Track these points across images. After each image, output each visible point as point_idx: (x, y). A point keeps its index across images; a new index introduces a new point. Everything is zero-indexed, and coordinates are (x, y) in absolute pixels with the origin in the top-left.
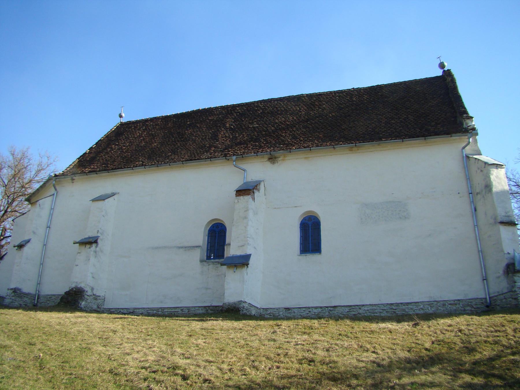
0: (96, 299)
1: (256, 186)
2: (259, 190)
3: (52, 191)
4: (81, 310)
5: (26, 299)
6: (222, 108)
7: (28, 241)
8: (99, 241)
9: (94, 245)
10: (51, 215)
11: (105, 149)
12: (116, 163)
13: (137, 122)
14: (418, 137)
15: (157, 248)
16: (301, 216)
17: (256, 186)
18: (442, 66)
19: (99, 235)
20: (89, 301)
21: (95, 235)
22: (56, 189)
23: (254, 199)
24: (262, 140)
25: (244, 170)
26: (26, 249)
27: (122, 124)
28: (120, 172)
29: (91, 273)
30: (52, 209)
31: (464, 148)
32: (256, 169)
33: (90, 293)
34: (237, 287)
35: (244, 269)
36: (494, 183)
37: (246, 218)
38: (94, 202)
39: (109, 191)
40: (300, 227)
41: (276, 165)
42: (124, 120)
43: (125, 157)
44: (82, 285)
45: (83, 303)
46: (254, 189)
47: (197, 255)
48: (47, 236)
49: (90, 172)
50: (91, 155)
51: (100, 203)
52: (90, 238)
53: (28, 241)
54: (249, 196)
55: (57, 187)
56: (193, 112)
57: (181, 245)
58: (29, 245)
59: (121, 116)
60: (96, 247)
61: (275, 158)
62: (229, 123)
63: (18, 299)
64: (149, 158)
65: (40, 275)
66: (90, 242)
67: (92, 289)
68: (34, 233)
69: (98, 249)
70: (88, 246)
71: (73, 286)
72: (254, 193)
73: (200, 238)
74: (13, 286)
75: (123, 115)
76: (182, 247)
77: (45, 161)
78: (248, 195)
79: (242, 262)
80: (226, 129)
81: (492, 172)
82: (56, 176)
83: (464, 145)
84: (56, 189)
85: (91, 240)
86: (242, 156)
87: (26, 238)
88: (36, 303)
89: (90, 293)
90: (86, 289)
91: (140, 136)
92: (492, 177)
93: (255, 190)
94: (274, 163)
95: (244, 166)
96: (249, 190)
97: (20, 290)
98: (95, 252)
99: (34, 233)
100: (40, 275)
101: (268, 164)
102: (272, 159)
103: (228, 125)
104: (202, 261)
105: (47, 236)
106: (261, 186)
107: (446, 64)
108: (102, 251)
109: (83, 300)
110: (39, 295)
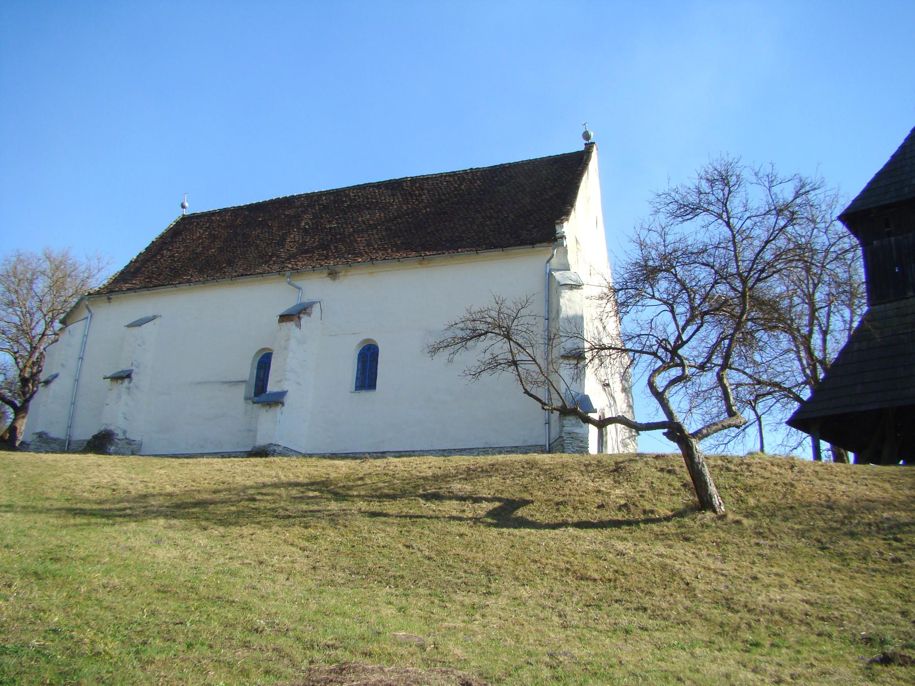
0: (130, 444)
1: (305, 309)
2: (309, 315)
3: (86, 313)
4: (110, 454)
5: (54, 445)
6: (307, 196)
7: (56, 376)
8: (133, 375)
9: (127, 381)
10: (84, 343)
11: (155, 256)
12: (162, 277)
13: (203, 215)
14: (496, 247)
15: (200, 383)
16: (359, 345)
17: (305, 309)
18: (586, 136)
19: (133, 368)
20: (120, 446)
21: (130, 368)
22: (90, 311)
23: (299, 326)
24: (332, 247)
25: (299, 288)
26: (52, 385)
27: (185, 219)
28: (161, 290)
29: (119, 412)
30: (86, 336)
31: (548, 261)
32: (314, 287)
33: (121, 436)
34: (270, 426)
35: (278, 409)
36: (563, 308)
37: (286, 348)
38: (131, 329)
39: (150, 314)
40: (359, 359)
41: (337, 281)
42: (186, 212)
43: (175, 268)
44: (112, 428)
45: (113, 448)
46: (300, 313)
47: (241, 392)
48: (79, 370)
49: (129, 289)
50: (137, 265)
51: (136, 329)
52: (123, 371)
53: (56, 376)
54: (292, 323)
55: (91, 309)
56: (278, 201)
57: (225, 380)
58: (57, 380)
59: (183, 207)
60: (130, 383)
61: (336, 273)
62: (306, 221)
63: (44, 445)
64: (201, 271)
65: (72, 417)
66: (123, 376)
67: (125, 432)
68: (63, 366)
69: (131, 385)
70: (120, 382)
71: (103, 428)
72: (299, 318)
73: (246, 370)
74: (39, 430)
75: (187, 204)
76: (226, 382)
77: (94, 263)
78: (292, 321)
79: (277, 400)
80: (299, 229)
81: (563, 294)
82: (90, 294)
83: (548, 257)
84: (90, 311)
85: (122, 374)
86: (296, 271)
87: (54, 372)
88: (66, 446)
89: (121, 436)
90: (116, 432)
91: (199, 238)
92: (562, 301)
93: (302, 315)
94: (334, 279)
95: (299, 283)
96: (293, 315)
97: (46, 434)
98: (129, 388)
99: (63, 366)
100: (72, 417)
101: (328, 281)
102: (333, 274)
103: (303, 224)
104: (246, 399)
105: (79, 370)
106: (314, 309)
107: (592, 134)
108: (137, 387)
109: (112, 445)
110: (69, 441)
